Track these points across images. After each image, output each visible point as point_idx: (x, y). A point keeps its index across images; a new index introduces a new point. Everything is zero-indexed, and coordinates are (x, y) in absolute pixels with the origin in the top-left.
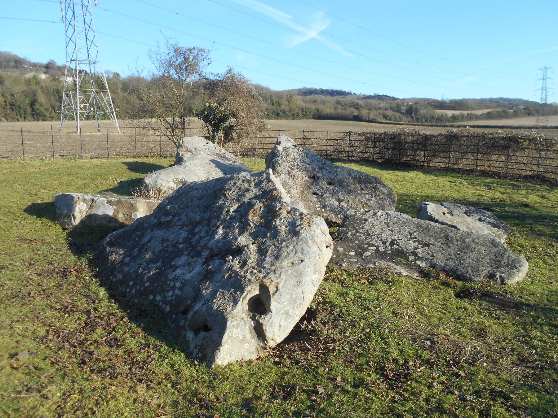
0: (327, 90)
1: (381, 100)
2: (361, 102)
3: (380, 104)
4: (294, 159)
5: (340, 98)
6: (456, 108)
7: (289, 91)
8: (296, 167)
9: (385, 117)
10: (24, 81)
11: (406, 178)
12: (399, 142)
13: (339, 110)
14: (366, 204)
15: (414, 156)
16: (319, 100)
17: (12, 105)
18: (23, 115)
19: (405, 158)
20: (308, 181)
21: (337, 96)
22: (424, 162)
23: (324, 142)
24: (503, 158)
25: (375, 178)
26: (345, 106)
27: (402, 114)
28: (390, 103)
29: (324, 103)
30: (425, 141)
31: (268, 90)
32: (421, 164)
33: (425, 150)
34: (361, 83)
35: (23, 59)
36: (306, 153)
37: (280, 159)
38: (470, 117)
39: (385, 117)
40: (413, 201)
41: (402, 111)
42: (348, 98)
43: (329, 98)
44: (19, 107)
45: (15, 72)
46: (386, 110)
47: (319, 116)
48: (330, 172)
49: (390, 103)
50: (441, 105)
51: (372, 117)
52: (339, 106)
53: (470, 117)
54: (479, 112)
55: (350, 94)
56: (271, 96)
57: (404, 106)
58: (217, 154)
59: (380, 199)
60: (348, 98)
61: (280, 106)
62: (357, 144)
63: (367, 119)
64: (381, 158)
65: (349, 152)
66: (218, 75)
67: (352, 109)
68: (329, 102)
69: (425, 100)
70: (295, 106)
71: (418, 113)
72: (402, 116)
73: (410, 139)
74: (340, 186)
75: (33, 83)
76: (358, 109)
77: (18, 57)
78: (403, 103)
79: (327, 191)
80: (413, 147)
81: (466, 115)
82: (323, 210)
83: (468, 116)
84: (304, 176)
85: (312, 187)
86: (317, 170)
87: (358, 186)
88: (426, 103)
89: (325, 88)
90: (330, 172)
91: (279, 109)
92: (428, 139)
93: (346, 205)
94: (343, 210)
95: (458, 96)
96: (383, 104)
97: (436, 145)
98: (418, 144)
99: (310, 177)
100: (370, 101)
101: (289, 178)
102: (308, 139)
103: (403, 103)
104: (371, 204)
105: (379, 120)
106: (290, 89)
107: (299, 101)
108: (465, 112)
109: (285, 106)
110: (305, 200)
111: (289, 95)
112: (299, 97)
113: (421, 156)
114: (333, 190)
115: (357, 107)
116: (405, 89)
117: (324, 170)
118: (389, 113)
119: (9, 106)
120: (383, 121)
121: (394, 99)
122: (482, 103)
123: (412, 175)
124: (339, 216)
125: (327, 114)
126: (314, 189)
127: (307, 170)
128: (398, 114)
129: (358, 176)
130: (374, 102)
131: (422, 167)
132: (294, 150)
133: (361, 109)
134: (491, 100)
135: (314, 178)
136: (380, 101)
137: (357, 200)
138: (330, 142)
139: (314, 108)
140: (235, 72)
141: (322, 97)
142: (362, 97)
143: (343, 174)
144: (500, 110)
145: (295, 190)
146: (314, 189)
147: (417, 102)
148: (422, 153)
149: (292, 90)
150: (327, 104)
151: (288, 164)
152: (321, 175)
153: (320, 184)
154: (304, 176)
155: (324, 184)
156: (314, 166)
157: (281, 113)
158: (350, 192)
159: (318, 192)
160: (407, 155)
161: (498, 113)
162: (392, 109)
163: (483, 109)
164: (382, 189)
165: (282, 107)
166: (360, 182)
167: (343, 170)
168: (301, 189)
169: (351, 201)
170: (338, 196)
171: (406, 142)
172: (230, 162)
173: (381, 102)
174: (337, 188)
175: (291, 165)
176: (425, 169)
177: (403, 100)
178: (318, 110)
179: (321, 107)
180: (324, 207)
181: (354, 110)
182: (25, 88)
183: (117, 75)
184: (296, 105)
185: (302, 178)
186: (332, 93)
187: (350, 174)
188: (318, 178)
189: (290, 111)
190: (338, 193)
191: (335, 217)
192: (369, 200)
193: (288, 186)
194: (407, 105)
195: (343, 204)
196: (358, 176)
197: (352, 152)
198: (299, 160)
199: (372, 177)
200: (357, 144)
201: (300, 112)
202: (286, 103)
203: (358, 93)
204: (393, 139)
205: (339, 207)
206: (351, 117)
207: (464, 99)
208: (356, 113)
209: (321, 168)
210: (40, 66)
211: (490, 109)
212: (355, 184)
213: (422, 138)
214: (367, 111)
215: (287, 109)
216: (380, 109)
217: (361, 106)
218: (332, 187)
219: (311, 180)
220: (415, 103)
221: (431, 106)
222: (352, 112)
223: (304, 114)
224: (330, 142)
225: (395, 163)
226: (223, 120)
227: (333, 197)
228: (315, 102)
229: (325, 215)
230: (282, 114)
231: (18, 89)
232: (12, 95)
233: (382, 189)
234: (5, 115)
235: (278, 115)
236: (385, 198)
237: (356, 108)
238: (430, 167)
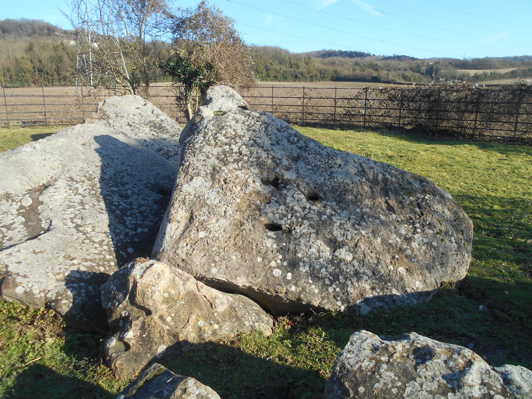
0: (346, 52)
1: (400, 60)
2: (379, 63)
3: (399, 64)
4: (234, 138)
5: (358, 59)
6: (479, 67)
7: (307, 54)
8: (235, 156)
9: (405, 78)
10: (52, 48)
11: (457, 158)
12: (437, 101)
13: (358, 72)
14: (401, 250)
15: (459, 120)
16: (337, 62)
17: (40, 71)
18: (51, 81)
19: (445, 124)
20: (258, 193)
21: (356, 58)
22: (475, 128)
23: (331, 102)
25: (422, 180)
26: (363, 67)
27: (422, 74)
28: (409, 63)
29: (342, 64)
30: (478, 99)
31: (287, 52)
32: (470, 132)
33: (477, 112)
34: (381, 42)
35: (55, 27)
36: (264, 123)
37: (200, 137)
38: (493, 76)
39: (405, 78)
40: (485, 212)
41: (422, 72)
42: (367, 59)
43: (347, 59)
44: (47, 73)
45: (48, 39)
46: (405, 70)
47: (337, 78)
48: (316, 169)
49: (409, 63)
50: (463, 64)
51: (391, 77)
52: (358, 68)
53: (493, 76)
54: (503, 71)
55: (369, 55)
56: (290, 59)
57: (424, 66)
58: (150, 122)
59: (435, 235)
60: (367, 59)
61: (298, 68)
62: (376, 105)
63: (386, 80)
64: (409, 124)
65: (365, 115)
66: (187, 11)
67: (371, 70)
68: (347, 63)
69: (446, 59)
70: (313, 68)
71: (439, 73)
72: (421, 76)
73: (454, 96)
74: (338, 203)
75: (60, 50)
76: (376, 70)
77: (50, 24)
78: (423, 63)
79: (305, 218)
80: (458, 109)
81: (489, 74)
82: (289, 276)
83: (491, 75)
84: (250, 180)
85: (269, 209)
86: (285, 162)
87: (381, 200)
88: (447, 62)
89: (343, 50)
90: (316, 169)
91: (297, 71)
92: (483, 96)
93: (349, 258)
94: (342, 271)
95: (481, 55)
96: (402, 65)
97: (496, 104)
98: (467, 103)
99: (265, 182)
100: (389, 62)
101: (212, 187)
102: (310, 98)
103: (423, 63)
104: (412, 250)
105: (398, 81)
106: (309, 51)
107: (318, 63)
108: (488, 71)
109: (303, 68)
110: (244, 248)
111: (308, 58)
112: (317, 59)
113: (470, 120)
114: (320, 214)
115: (375, 68)
116: (427, 47)
117: (301, 164)
118: (409, 73)
119: (37, 72)
120: (402, 82)
121: (413, 59)
122: (506, 62)
123: (464, 151)
124: (331, 290)
125: (345, 76)
126: (273, 213)
127: (260, 165)
128: (417, 75)
129: (380, 177)
130: (393, 62)
131: (472, 136)
132: (238, 116)
133: (380, 70)
134: (515, 58)
135: (276, 184)
136: (399, 62)
137: (379, 240)
138: (340, 103)
139: (332, 69)
140: (210, 5)
141: (341, 59)
142: (381, 58)
143: (347, 173)
144: (525, 68)
145: (222, 221)
146: (273, 213)
147: (438, 62)
148: (473, 116)
149: (311, 52)
150: (345, 65)
151: (216, 151)
152: (294, 177)
153: (289, 200)
154: (250, 180)
155: (297, 199)
156: (279, 154)
157: (299, 76)
158: (361, 220)
159: (283, 222)
160: (448, 120)
161: (524, 71)
162: (411, 69)
163: (508, 67)
164: (438, 207)
165: (300, 70)
166: (385, 192)
167: (347, 162)
168: (238, 216)
169: (363, 246)
170: (331, 233)
171: (448, 101)
172: (164, 136)
173: (401, 63)
174: (329, 211)
175: (224, 152)
176: (485, 144)
177: (423, 61)
178: (336, 72)
179: (339, 69)
180: (293, 265)
181: (373, 71)
182: (53, 54)
184: (315, 67)
185: (246, 185)
186: (351, 55)
187: (362, 172)
188: (286, 183)
189: (308, 73)
190: (332, 223)
191: (321, 292)
192: (408, 240)
193: (204, 210)
194: (427, 65)
195: (344, 254)
196: (380, 177)
197: (369, 116)
198: (247, 138)
199: (414, 177)
200: (376, 105)
201: (318, 74)
202: (304, 65)
203: (377, 54)
204: (429, 96)
205: (332, 262)
206: (370, 78)
207: (487, 57)
208: (375, 74)
209: (296, 159)
210: (71, 33)
211: (515, 67)
212: (373, 197)
213: (473, 94)
214: (386, 72)
215: (305, 71)
216: (399, 69)
217: (379, 67)
218: (317, 207)
219: (266, 190)
220: (436, 63)
221: (453, 65)
222: (371, 73)
223: (322, 76)
224: (340, 103)
225: (431, 131)
226: (195, 74)
227: (317, 233)
228: (333, 63)
229: (293, 288)
230: (301, 76)
231: (45, 56)
232: (40, 61)
233: (438, 207)
234: (34, 81)
235: (296, 77)
236: (446, 233)
237: (374, 69)
238: (484, 136)
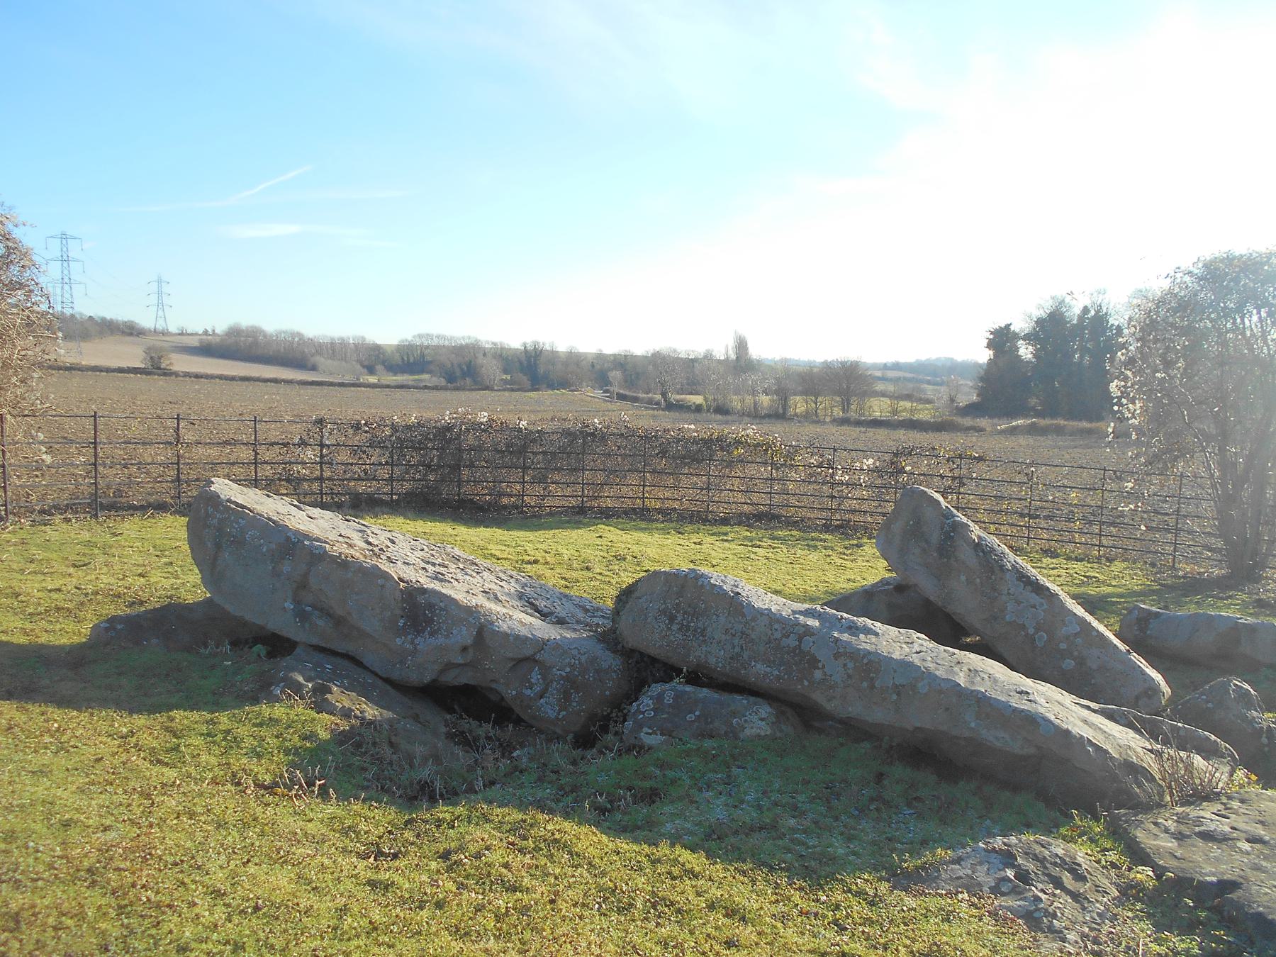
24: (700, 481)
92: (534, 441)
142: (194, 342)
183: (363, 338)
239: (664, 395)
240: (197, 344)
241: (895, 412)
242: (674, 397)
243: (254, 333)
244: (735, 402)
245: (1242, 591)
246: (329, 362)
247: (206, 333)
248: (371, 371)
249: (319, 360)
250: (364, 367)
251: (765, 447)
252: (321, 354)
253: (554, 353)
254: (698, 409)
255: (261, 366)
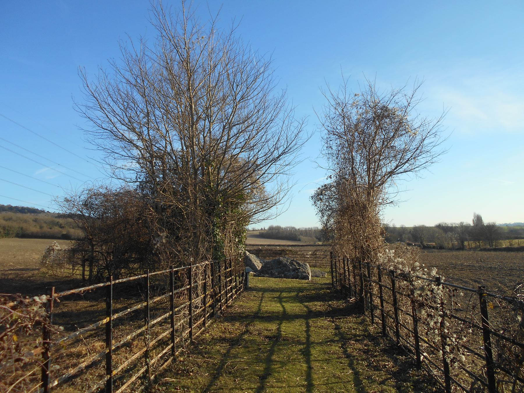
142: (257, 233)
239: (421, 243)
240: (258, 234)
241: (511, 245)
242: (425, 243)
243: (278, 228)
244: (446, 245)
245: (155, 244)
246: (305, 237)
247: (262, 229)
248: (320, 240)
249: (301, 237)
250: (317, 238)
251: (290, 251)
252: (302, 235)
253: (394, 229)
254: (434, 247)
255: (280, 241)
